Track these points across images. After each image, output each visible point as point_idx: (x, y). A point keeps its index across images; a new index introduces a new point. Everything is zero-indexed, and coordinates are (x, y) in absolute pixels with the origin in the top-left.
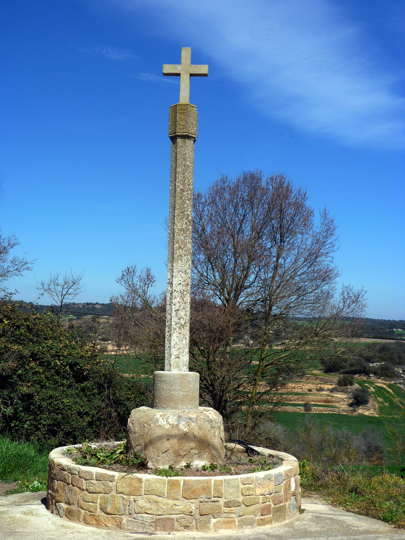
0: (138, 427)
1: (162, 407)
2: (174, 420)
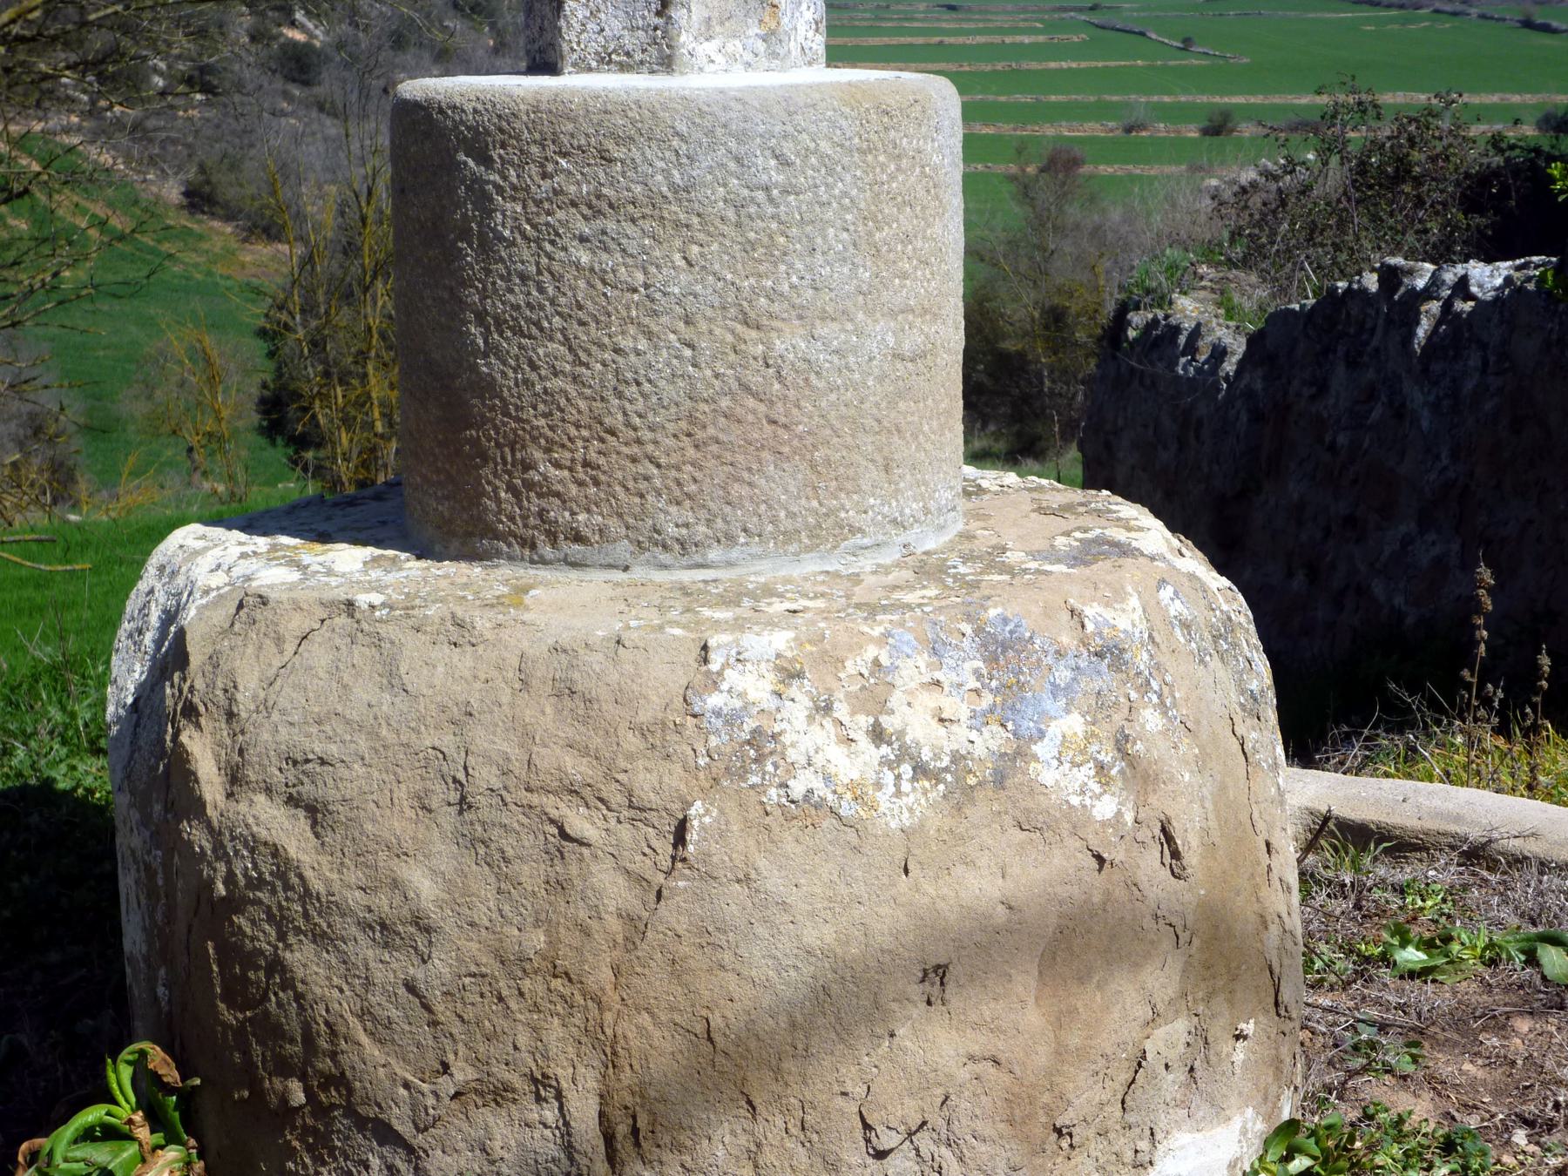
0: (445, 854)
1: (652, 542)
2: (956, 707)
